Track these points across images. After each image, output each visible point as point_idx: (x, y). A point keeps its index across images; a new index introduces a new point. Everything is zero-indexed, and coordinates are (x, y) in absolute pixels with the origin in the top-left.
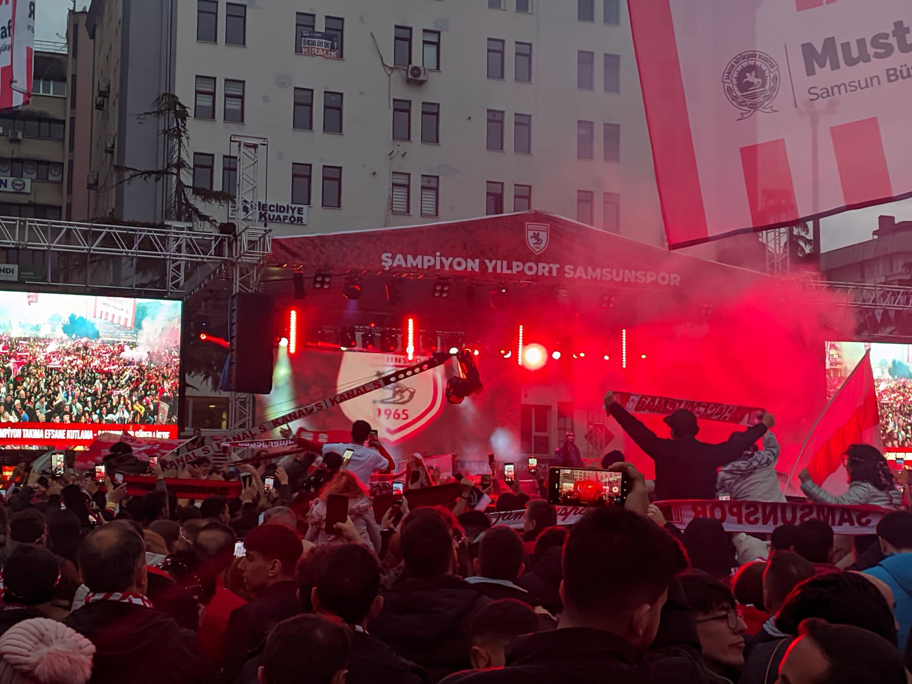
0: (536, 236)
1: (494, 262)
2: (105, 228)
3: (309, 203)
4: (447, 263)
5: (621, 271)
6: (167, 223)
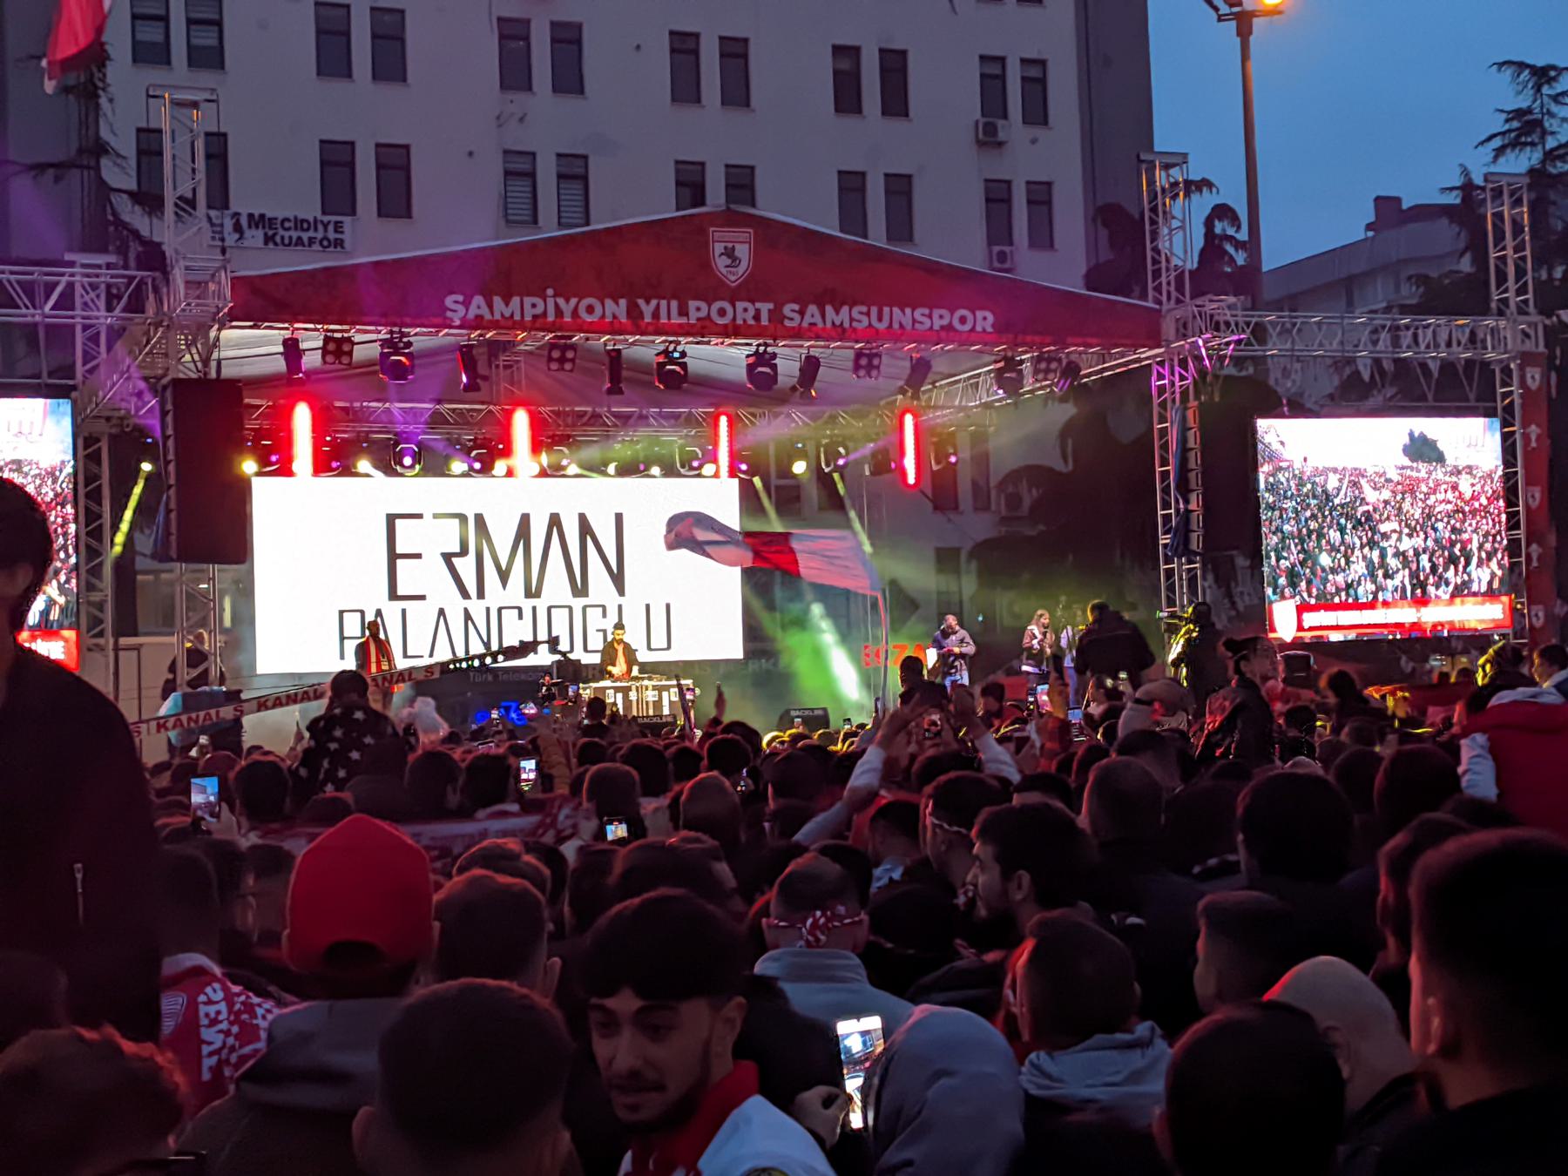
0: (730, 253)
1: (654, 302)
2: (62, 275)
3: (353, 213)
4: (567, 308)
5: (886, 310)
6: (68, 257)
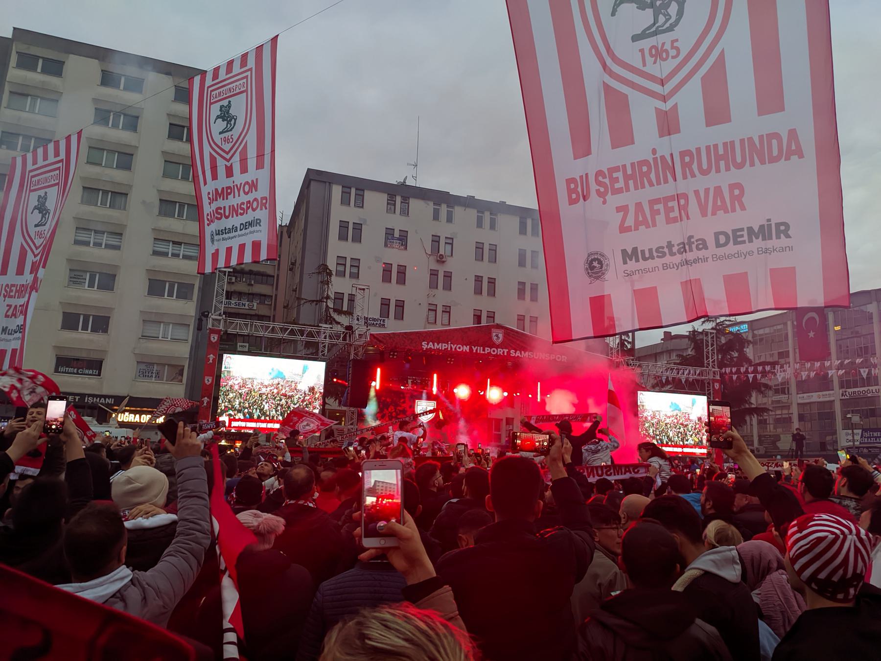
0: (497, 336)
4: (453, 348)
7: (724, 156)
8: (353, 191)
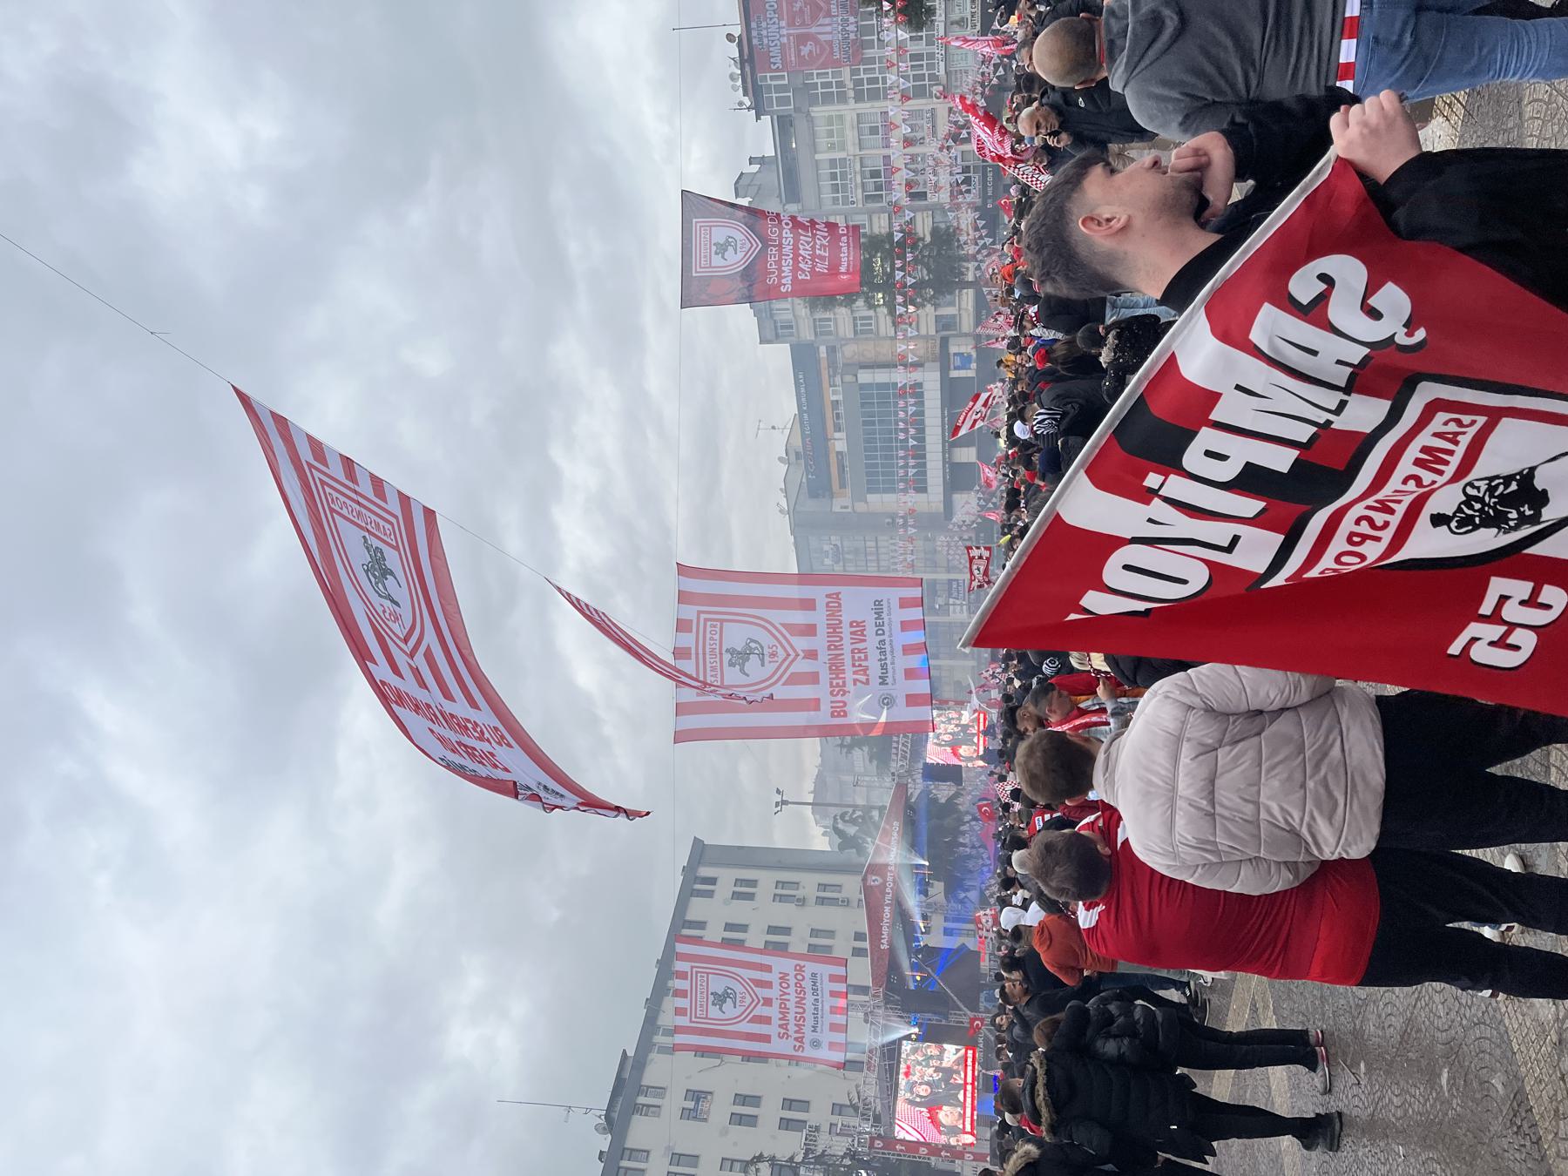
0: (722, 249)
7: (834, 629)
8: (624, 1163)
